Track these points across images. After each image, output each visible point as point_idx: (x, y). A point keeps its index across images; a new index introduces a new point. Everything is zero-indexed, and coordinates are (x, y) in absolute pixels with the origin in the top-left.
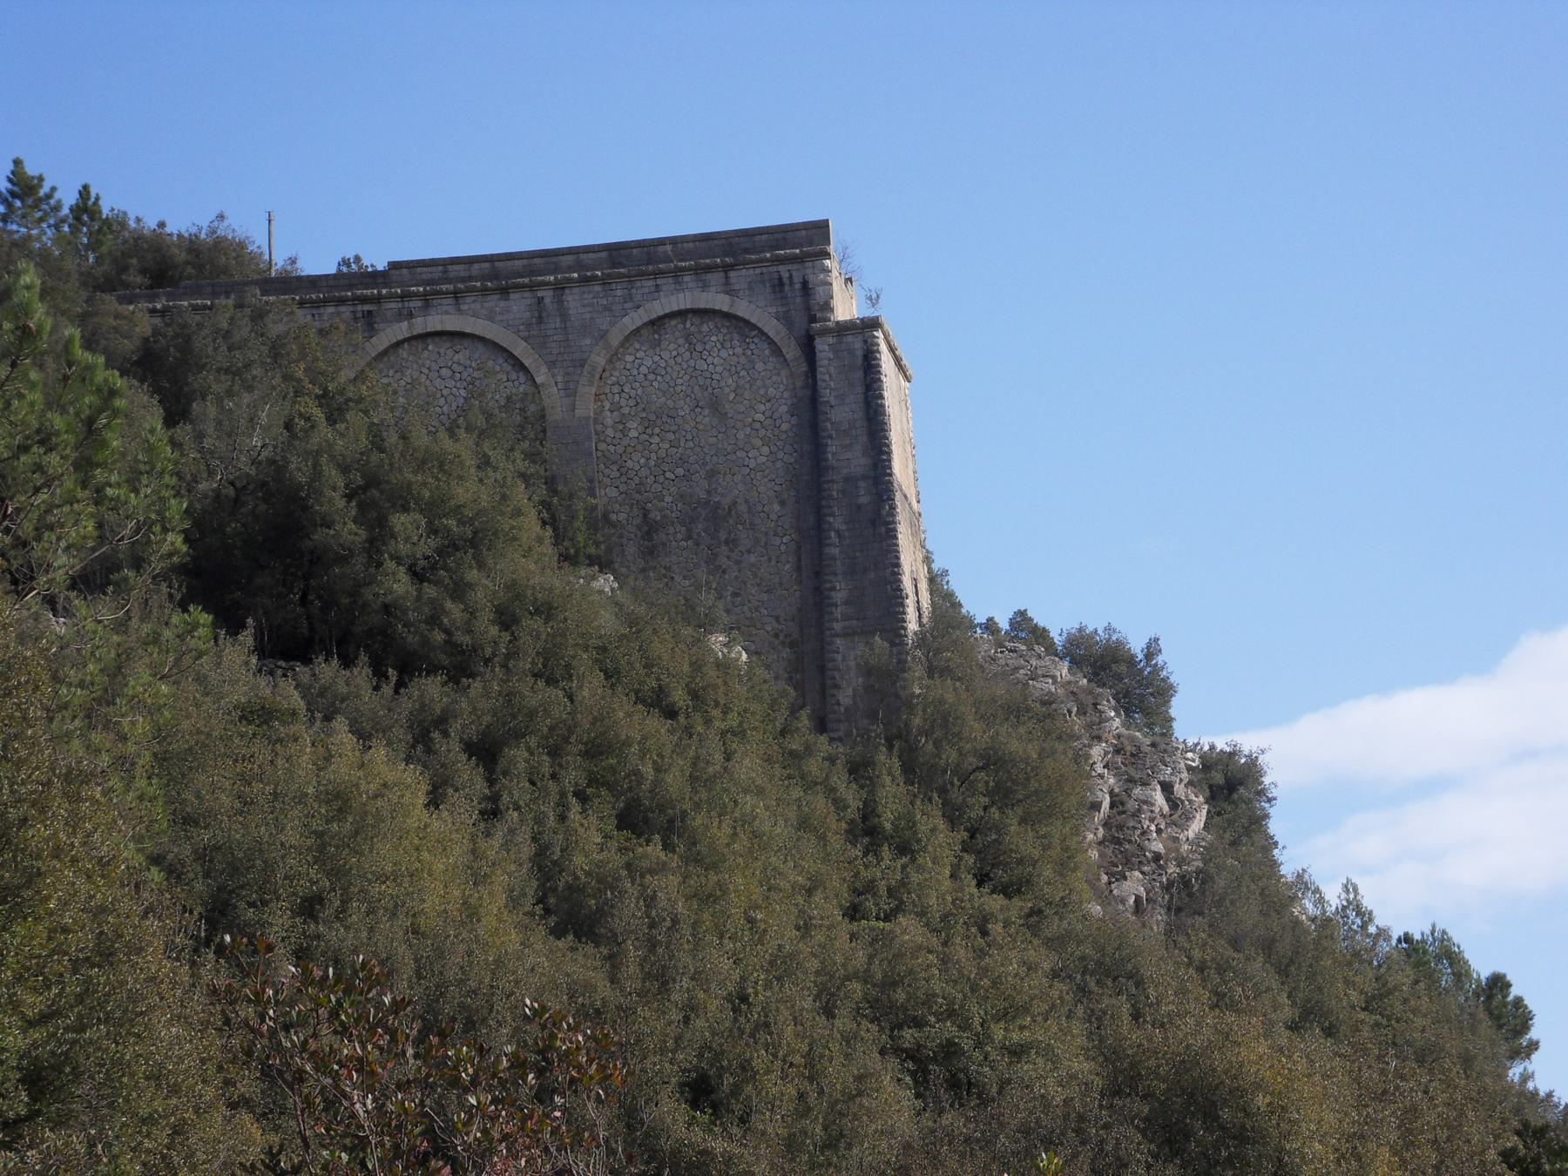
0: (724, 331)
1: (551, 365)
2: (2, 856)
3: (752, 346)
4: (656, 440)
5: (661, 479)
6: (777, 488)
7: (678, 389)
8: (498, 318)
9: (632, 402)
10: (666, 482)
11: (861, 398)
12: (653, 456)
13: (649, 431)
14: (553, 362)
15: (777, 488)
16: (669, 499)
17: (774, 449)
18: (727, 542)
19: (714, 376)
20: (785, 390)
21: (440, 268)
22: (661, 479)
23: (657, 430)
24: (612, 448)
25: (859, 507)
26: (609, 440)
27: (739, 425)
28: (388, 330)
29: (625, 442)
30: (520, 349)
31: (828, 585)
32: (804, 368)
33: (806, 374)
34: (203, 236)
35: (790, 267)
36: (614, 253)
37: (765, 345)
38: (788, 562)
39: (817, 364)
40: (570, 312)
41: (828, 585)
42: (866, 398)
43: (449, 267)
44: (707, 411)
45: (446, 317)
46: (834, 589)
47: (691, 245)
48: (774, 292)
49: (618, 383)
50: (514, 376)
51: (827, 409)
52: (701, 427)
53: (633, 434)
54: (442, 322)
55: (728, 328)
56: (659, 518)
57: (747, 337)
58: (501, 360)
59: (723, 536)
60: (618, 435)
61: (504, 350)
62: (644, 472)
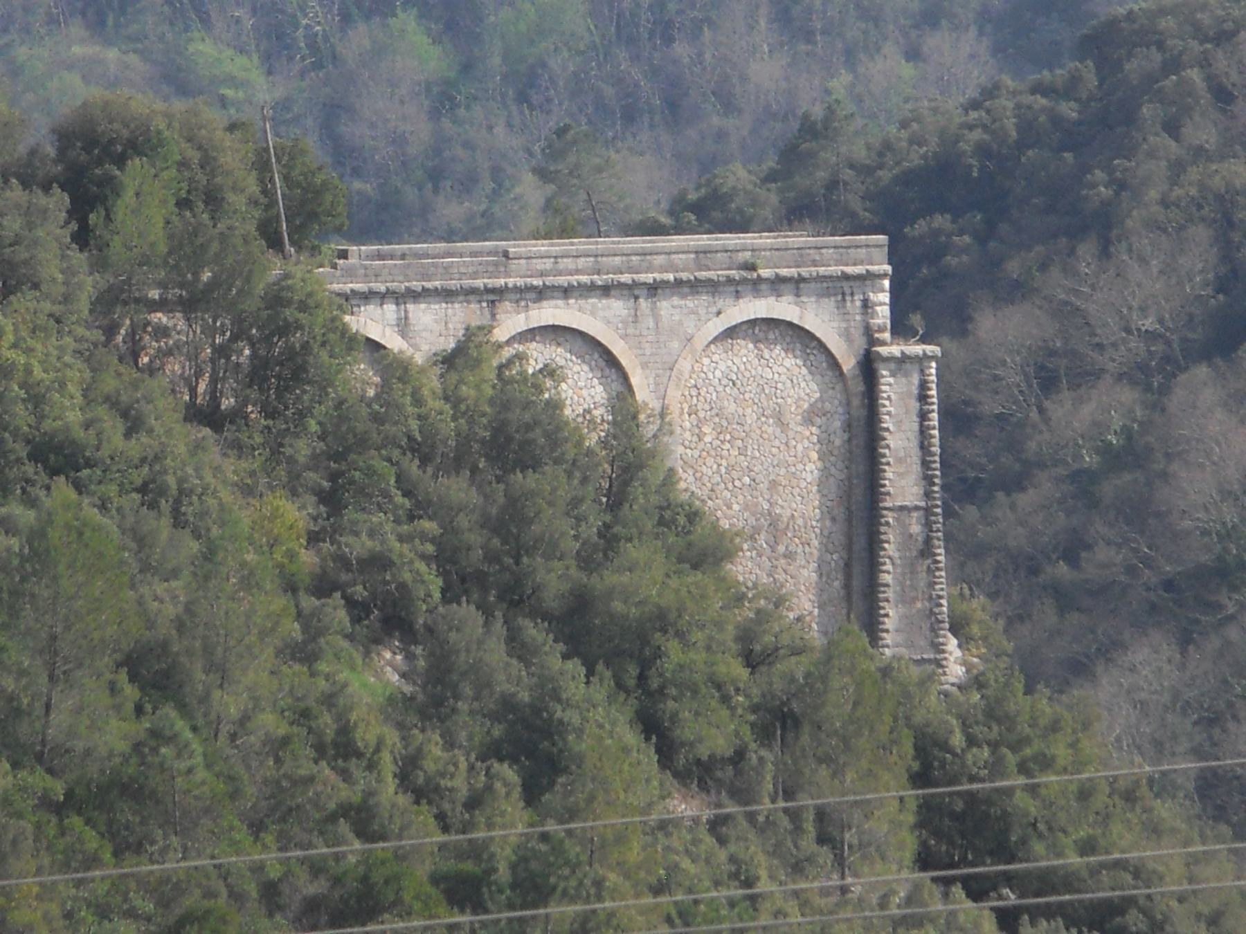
0: (788, 339)
1: (645, 366)
2: (30, 927)
3: (812, 357)
4: (727, 446)
5: (730, 486)
6: (829, 504)
7: (747, 396)
8: (601, 313)
9: (707, 407)
10: (736, 490)
11: (916, 427)
12: (724, 463)
13: (721, 437)
14: (646, 363)
15: (829, 504)
16: (736, 507)
17: (828, 465)
18: (785, 556)
19: (779, 385)
20: (746, 347)
21: (552, 260)
22: (730, 486)
23: (728, 437)
24: (688, 451)
25: (911, 536)
26: (687, 443)
27: (798, 437)
28: (509, 322)
29: (701, 446)
30: (618, 349)
31: (882, 612)
32: (861, 388)
33: (863, 394)
34: (729, 566)
35: (852, 283)
36: (701, 255)
37: (823, 358)
38: (837, 579)
39: (861, 378)
40: (662, 313)
41: (882, 612)
42: (921, 425)
43: (559, 260)
44: (771, 421)
45: (557, 311)
46: (887, 615)
47: (768, 253)
48: (838, 308)
49: (696, 386)
50: (607, 371)
51: (886, 434)
52: (765, 436)
53: (708, 439)
54: (554, 316)
55: (792, 337)
56: (727, 526)
57: (807, 347)
58: (596, 356)
59: (781, 549)
60: (695, 439)
61: (599, 344)
62: (717, 479)
